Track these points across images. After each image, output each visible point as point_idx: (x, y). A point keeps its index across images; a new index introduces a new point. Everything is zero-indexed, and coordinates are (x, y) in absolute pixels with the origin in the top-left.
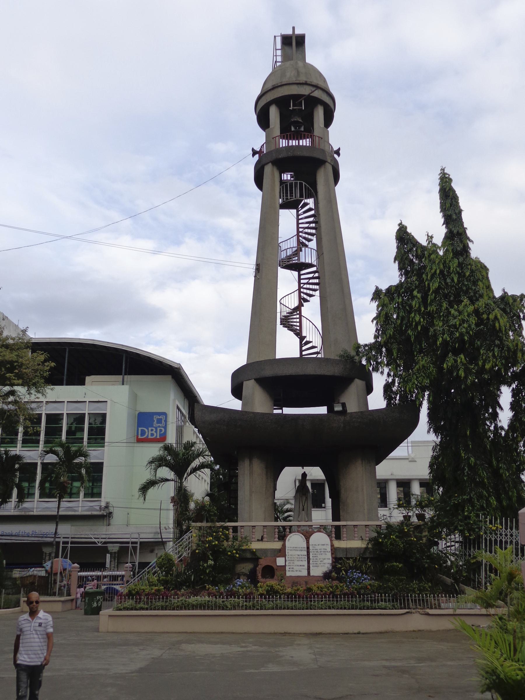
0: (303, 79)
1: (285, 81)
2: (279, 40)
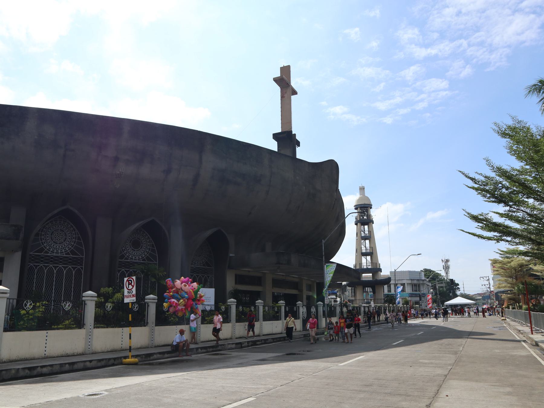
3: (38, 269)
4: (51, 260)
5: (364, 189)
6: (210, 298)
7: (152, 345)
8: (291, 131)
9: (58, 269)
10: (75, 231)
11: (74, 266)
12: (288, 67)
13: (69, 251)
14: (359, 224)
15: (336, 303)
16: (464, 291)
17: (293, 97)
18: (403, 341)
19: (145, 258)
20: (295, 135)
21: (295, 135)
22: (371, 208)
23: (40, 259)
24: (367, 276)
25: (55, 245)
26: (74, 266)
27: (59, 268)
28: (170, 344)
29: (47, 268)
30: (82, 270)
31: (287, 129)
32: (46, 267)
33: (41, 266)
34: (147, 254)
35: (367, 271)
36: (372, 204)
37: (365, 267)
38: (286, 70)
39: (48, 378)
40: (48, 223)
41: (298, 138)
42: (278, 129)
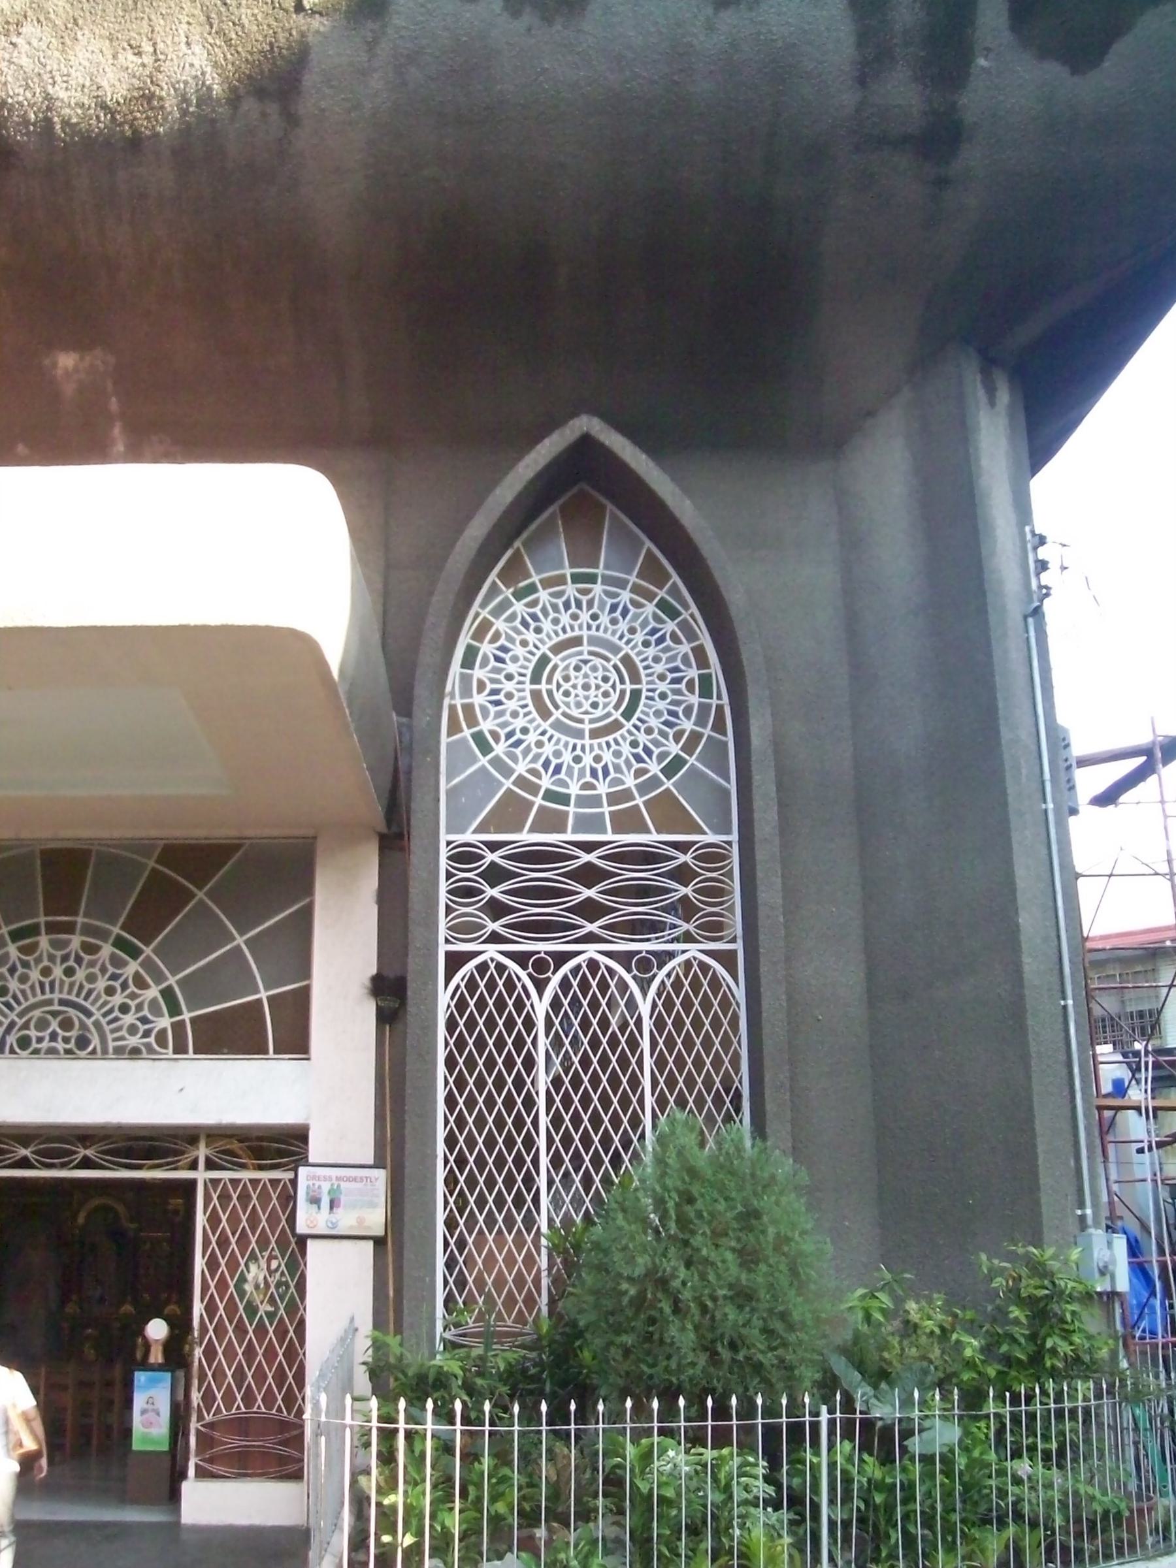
3: (659, 995)
4: (592, 893)
9: (565, 984)
10: (706, 692)
11: (542, 947)
13: (639, 801)
15: (1097, 1275)
16: (1162, 802)
17: (1072, 820)
19: (571, 809)
25: (617, 742)
26: (542, 947)
27: (482, 968)
28: (1148, 743)
29: (556, 980)
30: (11, 1046)
32: (540, 967)
33: (593, 965)
34: (479, 738)
40: (703, 662)
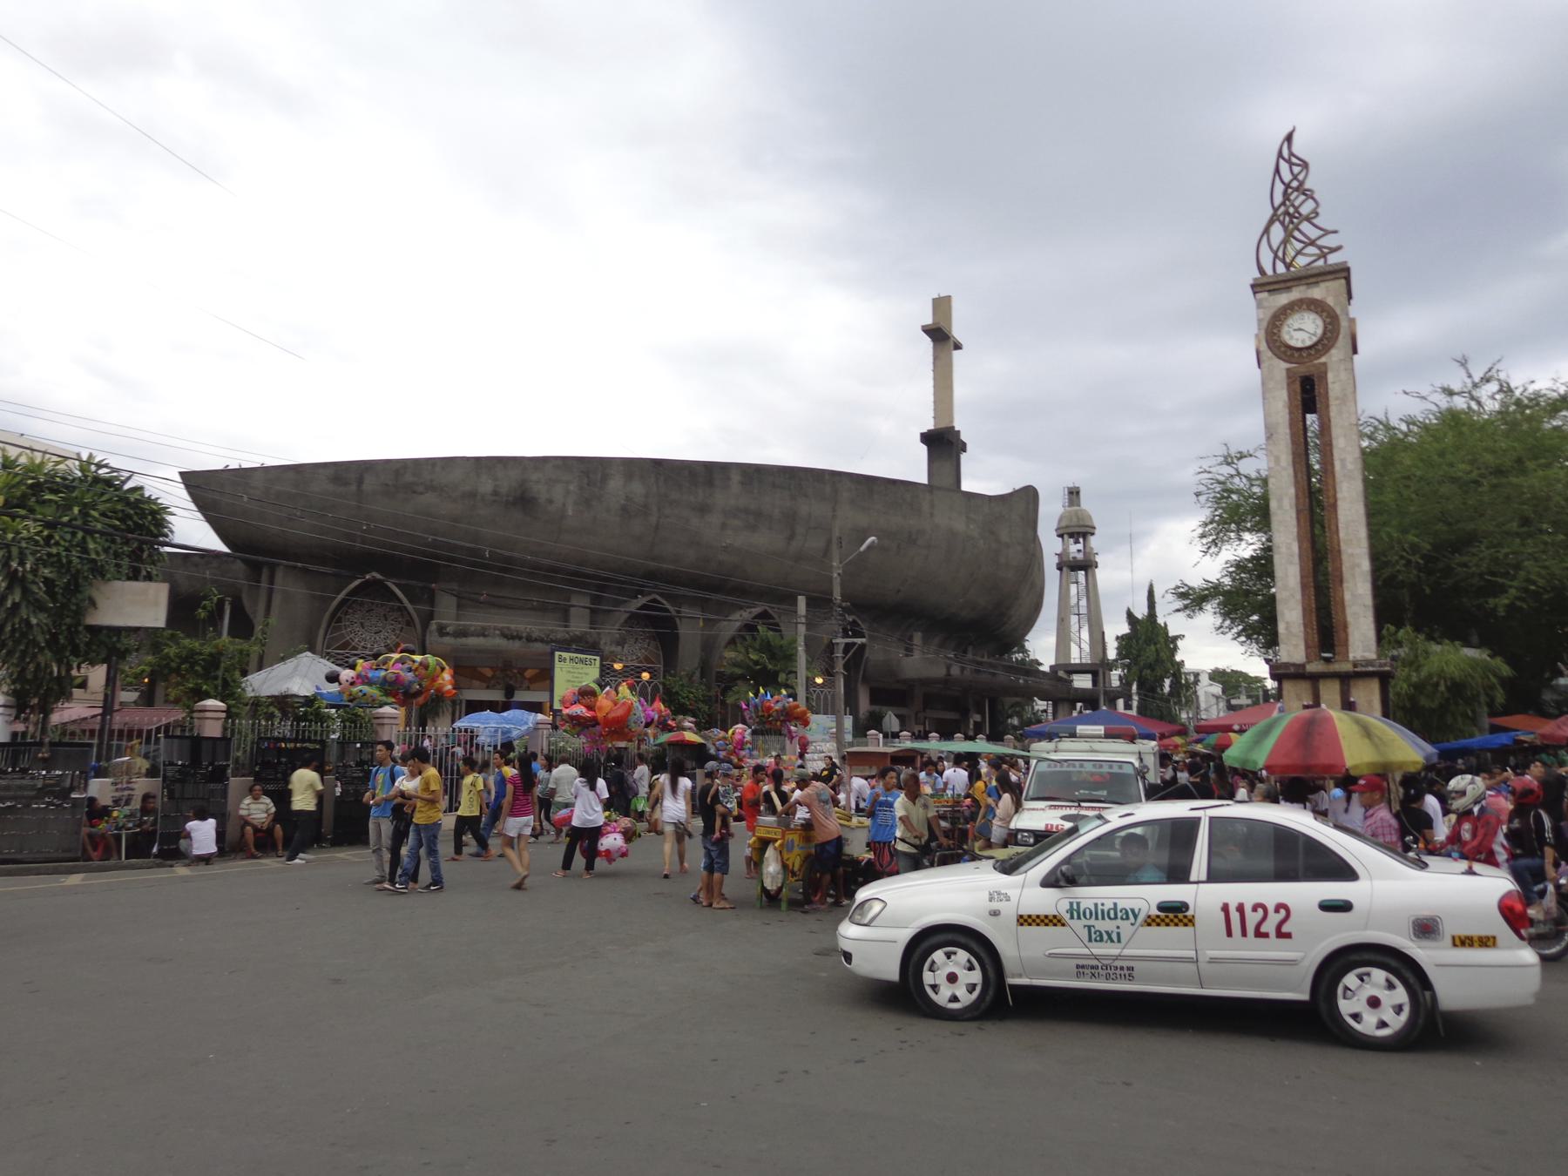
0: (1081, 523)
1: (1073, 524)
2: (1066, 490)
5: (1078, 493)
6: (1281, 934)
7: (995, 913)
8: (953, 427)
12: (948, 299)
14: (1065, 569)
18: (1533, 826)
20: (959, 432)
21: (959, 432)
22: (1096, 567)
23: (1055, 880)
24: (1083, 682)
31: (943, 425)
35: (1081, 669)
36: (1096, 525)
37: (1078, 661)
38: (942, 305)
39: (1390, 856)
41: (963, 437)
42: (929, 425)
